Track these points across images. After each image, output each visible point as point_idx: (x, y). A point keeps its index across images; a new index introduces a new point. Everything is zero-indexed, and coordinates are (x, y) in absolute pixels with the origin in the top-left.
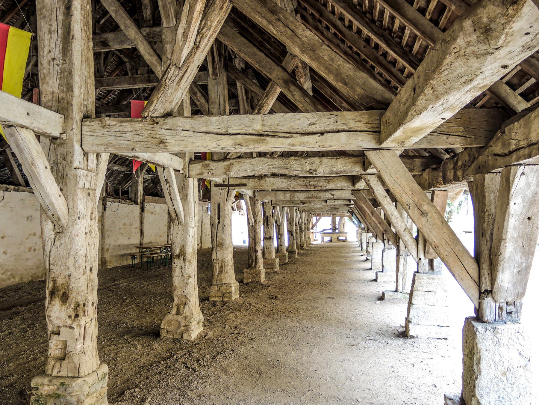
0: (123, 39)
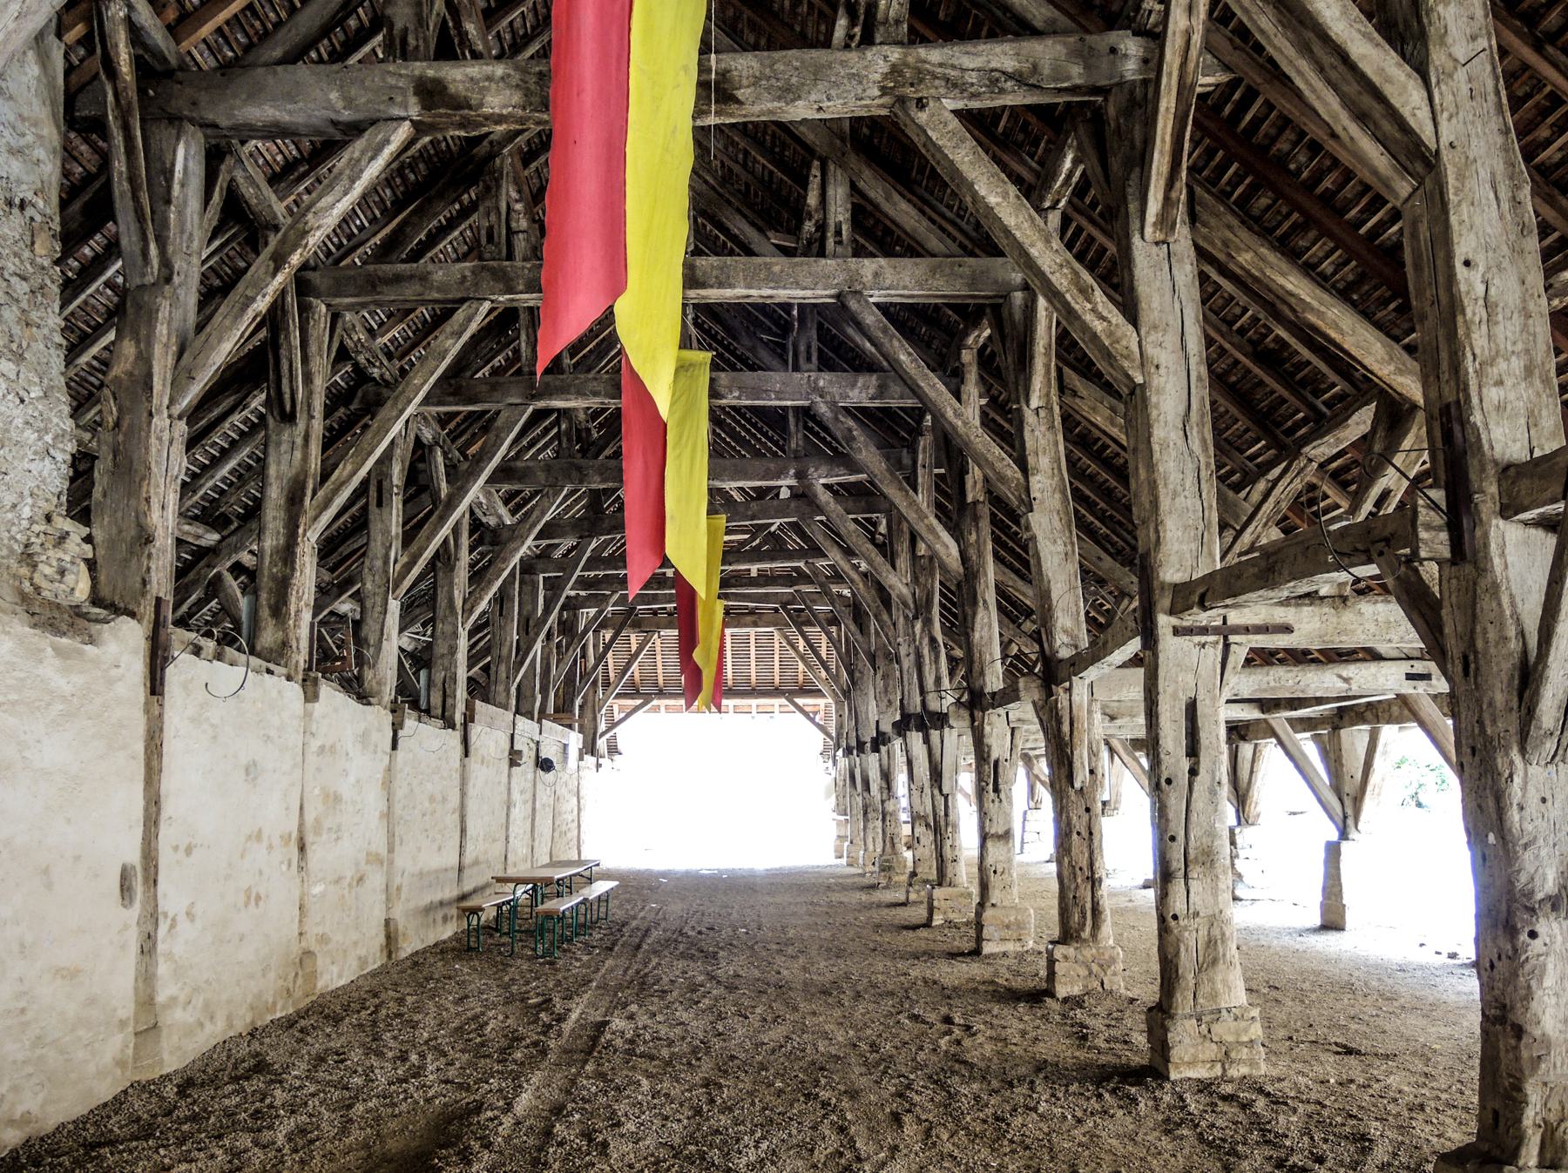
0: (794, 80)
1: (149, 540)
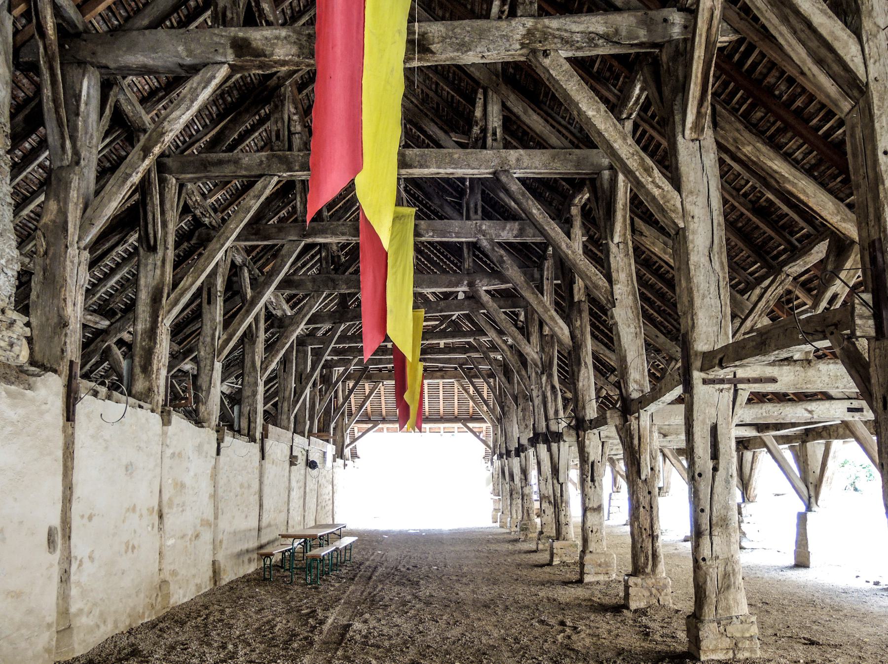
0: (467, 39)
1: (66, 325)
